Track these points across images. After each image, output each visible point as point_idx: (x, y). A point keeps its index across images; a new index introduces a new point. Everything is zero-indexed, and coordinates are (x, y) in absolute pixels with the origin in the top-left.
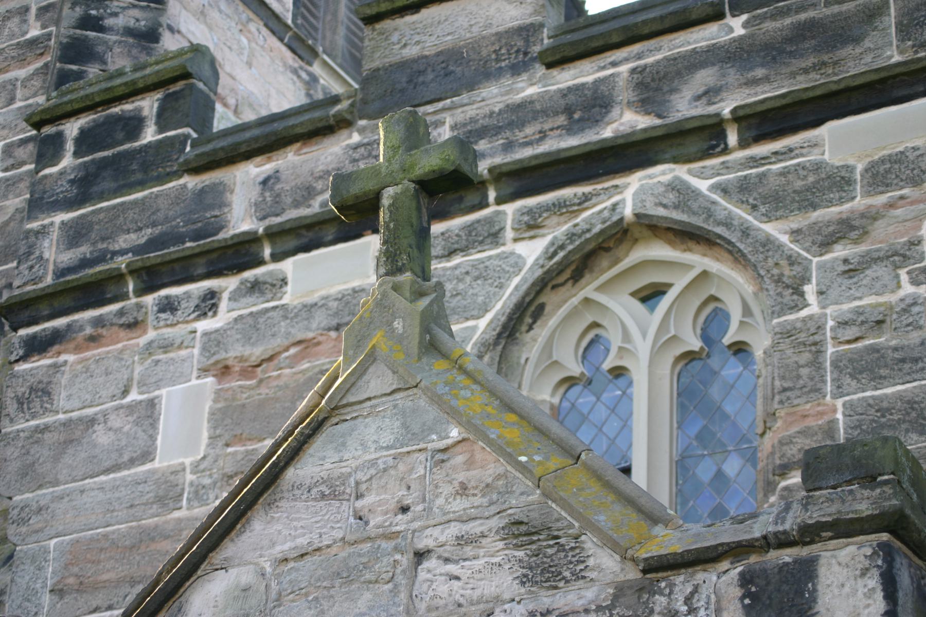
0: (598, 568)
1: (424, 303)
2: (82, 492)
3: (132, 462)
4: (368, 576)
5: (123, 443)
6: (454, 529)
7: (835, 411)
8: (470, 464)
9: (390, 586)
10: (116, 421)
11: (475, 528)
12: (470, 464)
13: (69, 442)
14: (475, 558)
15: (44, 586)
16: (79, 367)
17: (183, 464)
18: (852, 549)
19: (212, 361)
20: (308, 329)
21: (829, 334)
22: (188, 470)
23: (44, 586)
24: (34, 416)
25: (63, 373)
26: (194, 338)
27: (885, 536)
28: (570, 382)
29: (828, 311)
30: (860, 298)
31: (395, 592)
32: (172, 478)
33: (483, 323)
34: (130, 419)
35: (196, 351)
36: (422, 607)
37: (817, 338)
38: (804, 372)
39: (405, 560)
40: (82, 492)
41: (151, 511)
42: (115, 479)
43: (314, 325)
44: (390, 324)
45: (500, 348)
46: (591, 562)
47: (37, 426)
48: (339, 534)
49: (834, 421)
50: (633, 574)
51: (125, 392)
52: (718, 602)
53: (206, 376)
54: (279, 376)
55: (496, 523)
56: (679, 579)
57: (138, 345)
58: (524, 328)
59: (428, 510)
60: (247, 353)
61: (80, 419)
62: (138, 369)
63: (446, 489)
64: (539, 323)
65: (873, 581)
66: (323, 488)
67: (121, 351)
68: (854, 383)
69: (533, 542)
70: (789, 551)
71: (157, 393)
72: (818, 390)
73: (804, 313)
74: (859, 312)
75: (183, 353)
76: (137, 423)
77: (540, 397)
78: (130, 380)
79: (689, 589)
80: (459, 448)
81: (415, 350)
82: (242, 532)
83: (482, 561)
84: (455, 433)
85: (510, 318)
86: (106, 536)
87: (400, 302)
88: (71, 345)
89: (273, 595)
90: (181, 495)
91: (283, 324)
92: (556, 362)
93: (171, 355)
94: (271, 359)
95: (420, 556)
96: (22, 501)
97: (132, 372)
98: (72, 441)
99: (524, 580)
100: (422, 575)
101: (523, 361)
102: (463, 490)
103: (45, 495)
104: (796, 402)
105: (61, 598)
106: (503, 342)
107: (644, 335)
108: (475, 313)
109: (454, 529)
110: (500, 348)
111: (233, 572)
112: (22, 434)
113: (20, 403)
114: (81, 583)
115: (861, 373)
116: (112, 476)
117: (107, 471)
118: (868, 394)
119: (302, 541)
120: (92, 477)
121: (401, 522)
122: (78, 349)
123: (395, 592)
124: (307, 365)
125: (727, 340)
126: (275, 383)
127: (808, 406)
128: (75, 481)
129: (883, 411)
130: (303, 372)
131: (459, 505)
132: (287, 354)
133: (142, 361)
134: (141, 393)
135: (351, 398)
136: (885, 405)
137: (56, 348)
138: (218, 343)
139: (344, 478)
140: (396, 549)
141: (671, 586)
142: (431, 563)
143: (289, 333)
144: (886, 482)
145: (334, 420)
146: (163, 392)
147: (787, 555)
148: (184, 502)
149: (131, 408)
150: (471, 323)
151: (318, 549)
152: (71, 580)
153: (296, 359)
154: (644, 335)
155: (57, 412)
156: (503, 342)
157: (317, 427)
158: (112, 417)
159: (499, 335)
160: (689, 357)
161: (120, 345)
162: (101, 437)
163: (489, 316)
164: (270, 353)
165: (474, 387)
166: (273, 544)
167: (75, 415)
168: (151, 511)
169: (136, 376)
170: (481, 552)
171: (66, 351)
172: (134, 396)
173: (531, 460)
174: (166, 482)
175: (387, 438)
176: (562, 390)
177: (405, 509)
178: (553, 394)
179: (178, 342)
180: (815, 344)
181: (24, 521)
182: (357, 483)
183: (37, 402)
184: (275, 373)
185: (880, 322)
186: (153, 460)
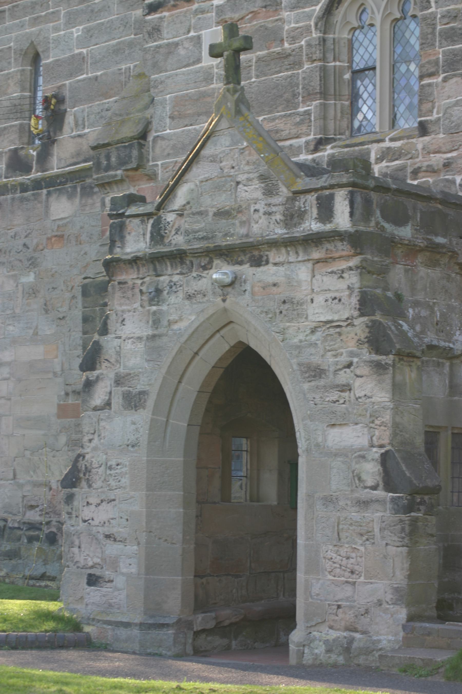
0: (282, 192)
1: (236, 96)
2: (177, 75)
3: (194, 63)
4: (224, 189)
5: (190, 54)
6: (246, 176)
7: (439, 53)
8: (250, 154)
9: (230, 192)
10: (186, 45)
11: (251, 176)
12: (250, 154)
13: (170, 53)
14: (252, 185)
15: (166, 115)
16: (170, 18)
17: (212, 65)
18: (343, 191)
19: (220, 19)
20: (255, 7)
21: (438, 21)
22: (215, 67)
23: (166, 115)
24: (155, 41)
25: (164, 22)
26: (212, 9)
27: (350, 189)
28: (354, 29)
29: (438, 10)
30: (449, 6)
31: (231, 194)
32: (209, 70)
33: (318, 8)
34: (191, 44)
35: (214, 14)
36: (239, 199)
37: (434, 22)
38: (429, 36)
39: (234, 184)
40: (177, 75)
41: (203, 85)
42: (188, 70)
43: (257, 5)
44: (227, 104)
45: (325, 19)
46: (280, 190)
47: (157, 45)
48: (216, 174)
49: (438, 59)
50: (291, 195)
51: (189, 32)
52: (311, 205)
53: (218, 26)
54: (246, 27)
55: (256, 175)
56: (302, 196)
57: (192, 9)
58: (334, 8)
59: (239, 168)
60: (233, 16)
61: (173, 43)
62: (193, 21)
63: (244, 162)
64: (340, 5)
65: (347, 202)
66: (211, 158)
67: (186, 12)
68: (446, 42)
69: (266, 182)
70: (328, 191)
71: (200, 32)
72: (433, 45)
73: (430, 11)
74: (448, 12)
75: (209, 14)
76: (194, 46)
77: (343, 36)
78: (190, 26)
79: (304, 200)
80: (247, 149)
81: (233, 114)
82: (190, 171)
83: (253, 187)
84: (245, 144)
85: (328, 6)
86: (187, 94)
87: (229, 96)
88: (166, 8)
89: (200, 193)
90: (213, 78)
91: (245, 4)
92: (348, 22)
93: (205, 15)
94: (242, 18)
95: (238, 183)
96: (154, 78)
97: (191, 22)
98: (170, 53)
99: (264, 194)
100: (239, 190)
101: (335, 22)
102: (248, 163)
103: (162, 76)
104: (426, 49)
105: (173, 120)
106: (326, 16)
107: (379, 12)
108: (315, 3)
109: (246, 176)
110: (325, 19)
111: (189, 184)
112: (152, 49)
113: (149, 35)
114: (180, 114)
115: (448, 38)
116: (187, 69)
117: (185, 66)
118: (450, 47)
119: (206, 175)
120: (180, 69)
121: (232, 172)
122: (169, 10)
123: (231, 194)
124: (255, 23)
125: (410, 14)
126: (244, 30)
127: (430, 51)
128: (173, 70)
129: (455, 55)
130: (254, 25)
131: (247, 168)
132: (248, 17)
133: (194, 17)
134: (195, 32)
135: (217, 129)
136: (455, 52)
137: (160, 10)
138: (222, 11)
139: (217, 155)
140: (231, 181)
141: (300, 199)
142: (240, 186)
143: (248, 8)
144: (351, 172)
145: (213, 135)
146: (203, 32)
147: (327, 192)
148: (215, 81)
149: (192, 38)
150: (313, 8)
151: (211, 179)
152: (176, 113)
153: (251, 20)
154: (379, 12)
155: (164, 39)
156: (326, 16)
157: (208, 138)
158: (185, 42)
159: (324, 14)
160: (397, 20)
161: (185, 9)
162: (182, 51)
163: (320, 5)
164: (241, 16)
165: (251, 127)
166: (199, 176)
167: (170, 40)
168: (203, 85)
169: (192, 24)
170: (253, 183)
171: (165, 11)
172: (192, 34)
173: (265, 156)
174: (207, 72)
175: (228, 143)
176: (352, 32)
177: (233, 168)
178: (348, 34)
179: (207, 9)
180: (433, 24)
181: (156, 87)
182: (221, 158)
183: (155, 35)
184: (244, 25)
185: (456, 17)
186: (201, 62)
